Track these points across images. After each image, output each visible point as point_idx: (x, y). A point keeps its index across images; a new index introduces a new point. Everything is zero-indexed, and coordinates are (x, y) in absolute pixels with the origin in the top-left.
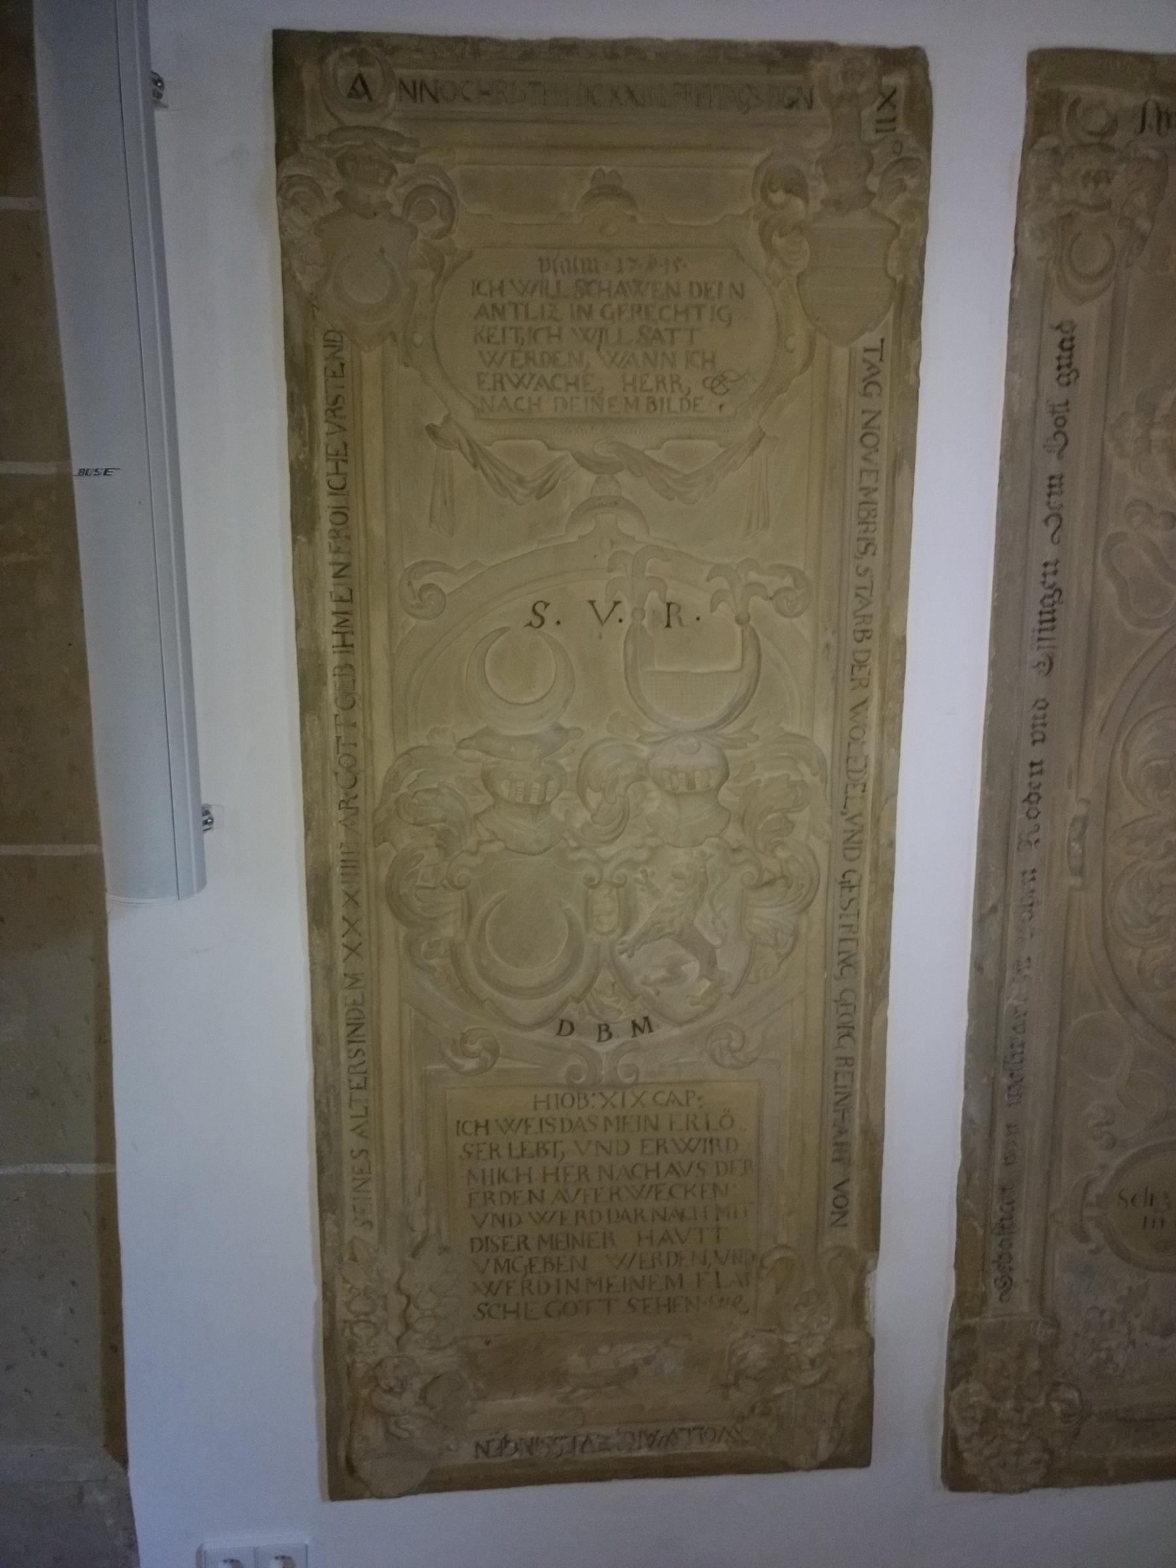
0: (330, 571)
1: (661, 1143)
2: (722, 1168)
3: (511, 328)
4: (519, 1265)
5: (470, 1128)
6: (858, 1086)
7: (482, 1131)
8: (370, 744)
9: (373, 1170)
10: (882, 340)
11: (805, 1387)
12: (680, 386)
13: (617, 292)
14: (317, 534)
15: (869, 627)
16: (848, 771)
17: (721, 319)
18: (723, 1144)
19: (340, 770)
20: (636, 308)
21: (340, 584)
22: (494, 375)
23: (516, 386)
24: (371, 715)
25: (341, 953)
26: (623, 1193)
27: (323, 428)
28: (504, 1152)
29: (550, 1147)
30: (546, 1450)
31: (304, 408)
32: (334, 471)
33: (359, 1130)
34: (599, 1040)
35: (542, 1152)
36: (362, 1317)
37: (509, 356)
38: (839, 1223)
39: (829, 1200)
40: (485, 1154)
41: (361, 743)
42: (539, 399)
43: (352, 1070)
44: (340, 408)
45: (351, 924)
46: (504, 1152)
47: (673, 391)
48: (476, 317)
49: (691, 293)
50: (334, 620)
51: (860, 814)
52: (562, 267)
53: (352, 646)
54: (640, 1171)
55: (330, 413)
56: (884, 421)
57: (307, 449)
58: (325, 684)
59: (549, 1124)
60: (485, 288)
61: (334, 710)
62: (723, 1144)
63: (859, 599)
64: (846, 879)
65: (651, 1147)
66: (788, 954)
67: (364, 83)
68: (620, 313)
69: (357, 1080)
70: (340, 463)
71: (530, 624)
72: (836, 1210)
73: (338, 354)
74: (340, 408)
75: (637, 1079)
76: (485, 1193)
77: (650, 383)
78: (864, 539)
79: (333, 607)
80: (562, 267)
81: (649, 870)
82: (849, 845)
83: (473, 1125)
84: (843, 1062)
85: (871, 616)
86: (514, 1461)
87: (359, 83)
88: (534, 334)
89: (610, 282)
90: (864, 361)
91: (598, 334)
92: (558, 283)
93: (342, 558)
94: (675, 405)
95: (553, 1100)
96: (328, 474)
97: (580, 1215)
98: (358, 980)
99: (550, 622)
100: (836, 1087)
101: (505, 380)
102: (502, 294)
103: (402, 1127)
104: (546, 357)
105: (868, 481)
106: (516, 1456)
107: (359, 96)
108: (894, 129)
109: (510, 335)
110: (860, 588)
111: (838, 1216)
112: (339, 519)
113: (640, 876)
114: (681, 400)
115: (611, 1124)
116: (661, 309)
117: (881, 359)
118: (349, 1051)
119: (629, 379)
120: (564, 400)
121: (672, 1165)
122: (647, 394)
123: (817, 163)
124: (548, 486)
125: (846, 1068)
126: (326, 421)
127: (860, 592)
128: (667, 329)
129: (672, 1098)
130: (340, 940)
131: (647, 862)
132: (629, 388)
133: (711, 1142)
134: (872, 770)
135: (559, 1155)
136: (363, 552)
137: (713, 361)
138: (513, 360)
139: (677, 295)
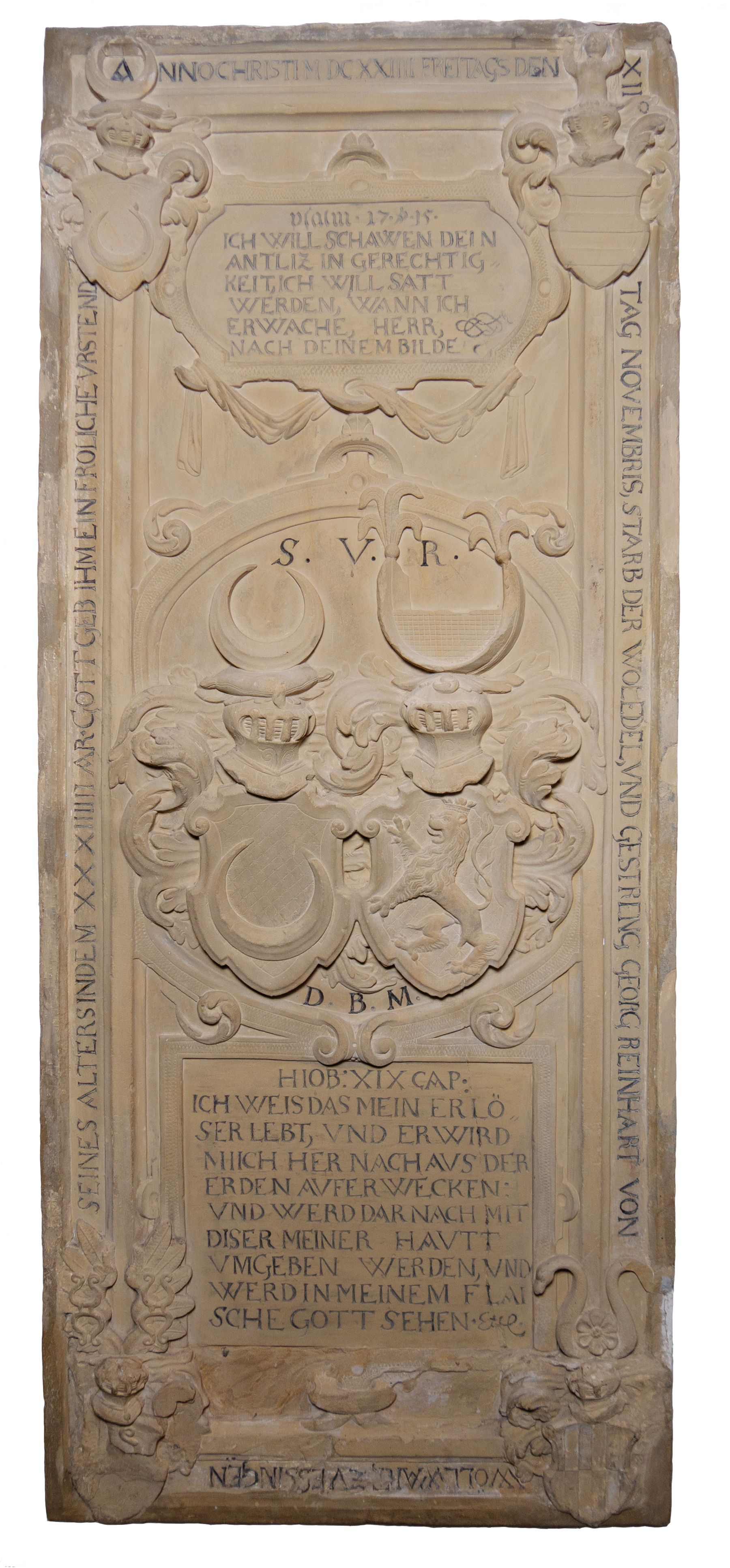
0: (76, 507)
1: (422, 1130)
2: (492, 1163)
3: (262, 277)
4: (262, 1265)
5: (208, 1104)
6: (644, 1071)
7: (221, 1108)
8: (108, 680)
9: (102, 1145)
10: (640, 283)
11: (590, 1422)
12: (433, 329)
13: (368, 242)
14: (64, 472)
15: (638, 567)
16: (623, 718)
17: (474, 266)
18: (492, 1134)
19: (78, 709)
20: (387, 257)
21: (84, 521)
22: (245, 321)
23: (267, 331)
24: (110, 651)
25: (72, 902)
26: (379, 1187)
27: (74, 372)
28: (245, 1133)
29: (296, 1130)
30: (291, 1483)
31: (56, 352)
32: (84, 412)
33: (86, 1099)
34: (352, 1011)
35: (288, 1135)
36: (85, 1311)
37: (259, 303)
38: (627, 1232)
39: (616, 1205)
40: (225, 1134)
41: (99, 679)
42: (290, 342)
43: (81, 1031)
44: (92, 353)
45: (84, 873)
46: (245, 1133)
47: (425, 333)
48: (227, 268)
49: (443, 241)
50: (77, 556)
51: (638, 765)
52: (313, 221)
53: (94, 581)
54: (397, 1162)
55: (81, 358)
56: (644, 360)
57: (57, 391)
58: (65, 619)
59: (296, 1104)
60: (237, 241)
61: (73, 646)
62: (492, 1134)
63: (627, 537)
64: (625, 836)
65: (411, 1135)
66: (561, 921)
67: (127, 69)
68: (371, 261)
69: (86, 1042)
70: (90, 404)
71: (278, 562)
72: (623, 1216)
73: (92, 304)
74: (92, 353)
75: (393, 1055)
76: (224, 1179)
77: (403, 326)
78: (629, 477)
79: (77, 543)
80: (313, 221)
81: (404, 821)
82: (626, 799)
83: (212, 1100)
84: (628, 1043)
85: (640, 555)
86: (253, 1492)
87: (123, 67)
88: (285, 282)
89: (361, 234)
90: (622, 302)
91: (349, 280)
92: (309, 235)
93: (87, 496)
94: (428, 347)
95: (300, 1077)
96: (77, 415)
97: (329, 1210)
98: (89, 933)
99: (299, 559)
100: (620, 1072)
101: (256, 325)
102: (254, 246)
103: (133, 1096)
104: (297, 303)
105: (632, 419)
106: (256, 1487)
107: (122, 79)
108: (641, 93)
109: (261, 283)
110: (628, 526)
111: (626, 1223)
112: (87, 457)
113: (394, 826)
114: (434, 341)
115: (365, 1107)
116: (413, 257)
117: (639, 302)
118: (79, 1010)
119: (380, 323)
120: (315, 343)
121: (434, 1156)
122: (400, 337)
123: (564, 122)
124: (298, 425)
125: (631, 1051)
126: (78, 365)
127: (627, 530)
128: (418, 276)
129: (434, 1079)
130: (71, 889)
131: (401, 810)
132: (381, 331)
133: (478, 1132)
134: (648, 716)
135: (307, 1140)
136: (108, 490)
137: (466, 305)
138: (264, 305)
139: (428, 243)
